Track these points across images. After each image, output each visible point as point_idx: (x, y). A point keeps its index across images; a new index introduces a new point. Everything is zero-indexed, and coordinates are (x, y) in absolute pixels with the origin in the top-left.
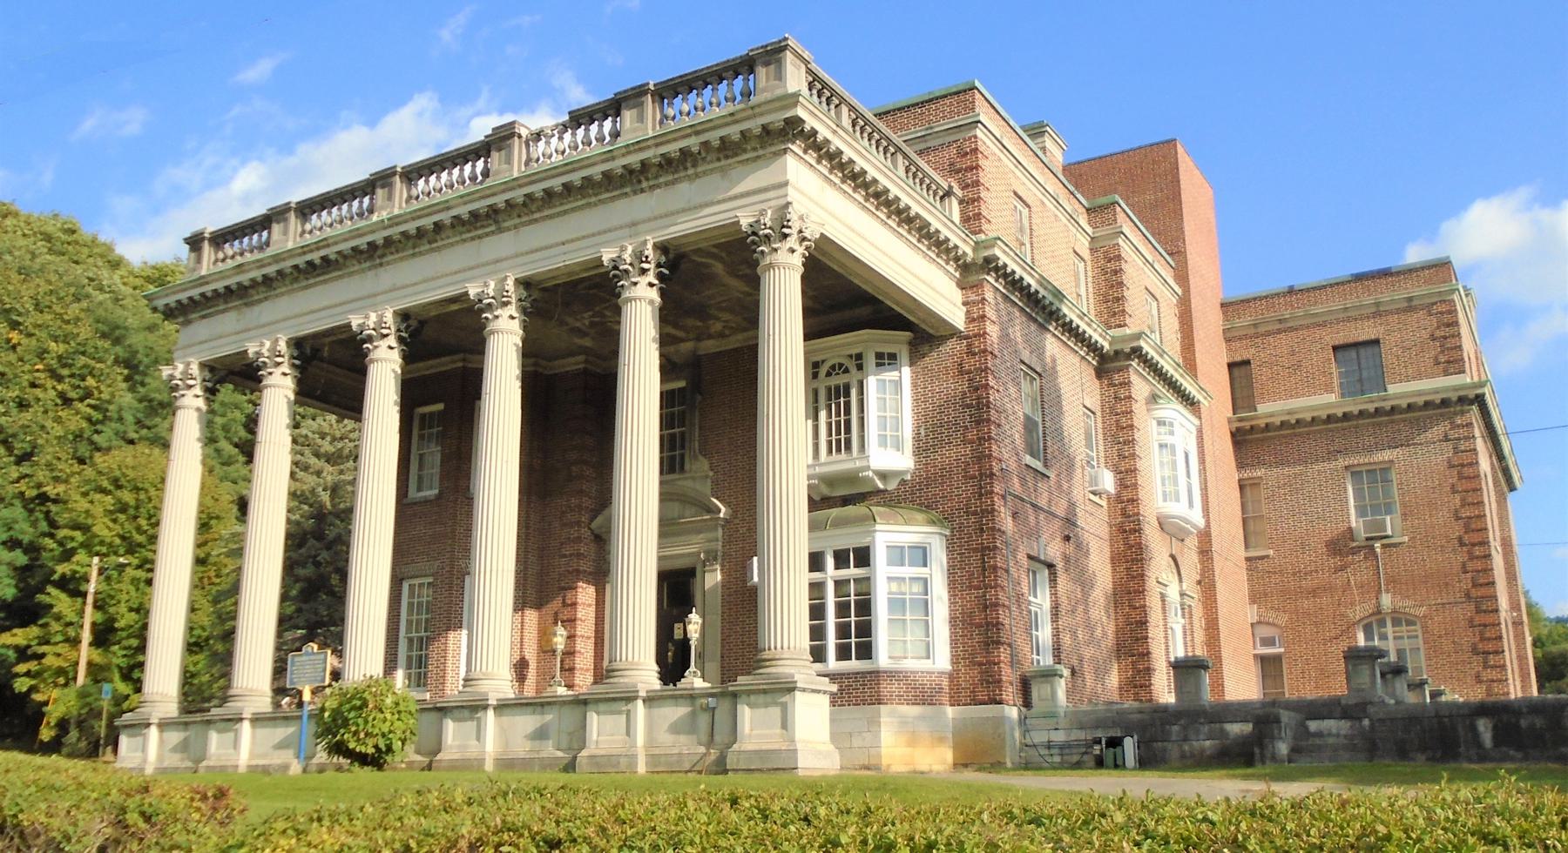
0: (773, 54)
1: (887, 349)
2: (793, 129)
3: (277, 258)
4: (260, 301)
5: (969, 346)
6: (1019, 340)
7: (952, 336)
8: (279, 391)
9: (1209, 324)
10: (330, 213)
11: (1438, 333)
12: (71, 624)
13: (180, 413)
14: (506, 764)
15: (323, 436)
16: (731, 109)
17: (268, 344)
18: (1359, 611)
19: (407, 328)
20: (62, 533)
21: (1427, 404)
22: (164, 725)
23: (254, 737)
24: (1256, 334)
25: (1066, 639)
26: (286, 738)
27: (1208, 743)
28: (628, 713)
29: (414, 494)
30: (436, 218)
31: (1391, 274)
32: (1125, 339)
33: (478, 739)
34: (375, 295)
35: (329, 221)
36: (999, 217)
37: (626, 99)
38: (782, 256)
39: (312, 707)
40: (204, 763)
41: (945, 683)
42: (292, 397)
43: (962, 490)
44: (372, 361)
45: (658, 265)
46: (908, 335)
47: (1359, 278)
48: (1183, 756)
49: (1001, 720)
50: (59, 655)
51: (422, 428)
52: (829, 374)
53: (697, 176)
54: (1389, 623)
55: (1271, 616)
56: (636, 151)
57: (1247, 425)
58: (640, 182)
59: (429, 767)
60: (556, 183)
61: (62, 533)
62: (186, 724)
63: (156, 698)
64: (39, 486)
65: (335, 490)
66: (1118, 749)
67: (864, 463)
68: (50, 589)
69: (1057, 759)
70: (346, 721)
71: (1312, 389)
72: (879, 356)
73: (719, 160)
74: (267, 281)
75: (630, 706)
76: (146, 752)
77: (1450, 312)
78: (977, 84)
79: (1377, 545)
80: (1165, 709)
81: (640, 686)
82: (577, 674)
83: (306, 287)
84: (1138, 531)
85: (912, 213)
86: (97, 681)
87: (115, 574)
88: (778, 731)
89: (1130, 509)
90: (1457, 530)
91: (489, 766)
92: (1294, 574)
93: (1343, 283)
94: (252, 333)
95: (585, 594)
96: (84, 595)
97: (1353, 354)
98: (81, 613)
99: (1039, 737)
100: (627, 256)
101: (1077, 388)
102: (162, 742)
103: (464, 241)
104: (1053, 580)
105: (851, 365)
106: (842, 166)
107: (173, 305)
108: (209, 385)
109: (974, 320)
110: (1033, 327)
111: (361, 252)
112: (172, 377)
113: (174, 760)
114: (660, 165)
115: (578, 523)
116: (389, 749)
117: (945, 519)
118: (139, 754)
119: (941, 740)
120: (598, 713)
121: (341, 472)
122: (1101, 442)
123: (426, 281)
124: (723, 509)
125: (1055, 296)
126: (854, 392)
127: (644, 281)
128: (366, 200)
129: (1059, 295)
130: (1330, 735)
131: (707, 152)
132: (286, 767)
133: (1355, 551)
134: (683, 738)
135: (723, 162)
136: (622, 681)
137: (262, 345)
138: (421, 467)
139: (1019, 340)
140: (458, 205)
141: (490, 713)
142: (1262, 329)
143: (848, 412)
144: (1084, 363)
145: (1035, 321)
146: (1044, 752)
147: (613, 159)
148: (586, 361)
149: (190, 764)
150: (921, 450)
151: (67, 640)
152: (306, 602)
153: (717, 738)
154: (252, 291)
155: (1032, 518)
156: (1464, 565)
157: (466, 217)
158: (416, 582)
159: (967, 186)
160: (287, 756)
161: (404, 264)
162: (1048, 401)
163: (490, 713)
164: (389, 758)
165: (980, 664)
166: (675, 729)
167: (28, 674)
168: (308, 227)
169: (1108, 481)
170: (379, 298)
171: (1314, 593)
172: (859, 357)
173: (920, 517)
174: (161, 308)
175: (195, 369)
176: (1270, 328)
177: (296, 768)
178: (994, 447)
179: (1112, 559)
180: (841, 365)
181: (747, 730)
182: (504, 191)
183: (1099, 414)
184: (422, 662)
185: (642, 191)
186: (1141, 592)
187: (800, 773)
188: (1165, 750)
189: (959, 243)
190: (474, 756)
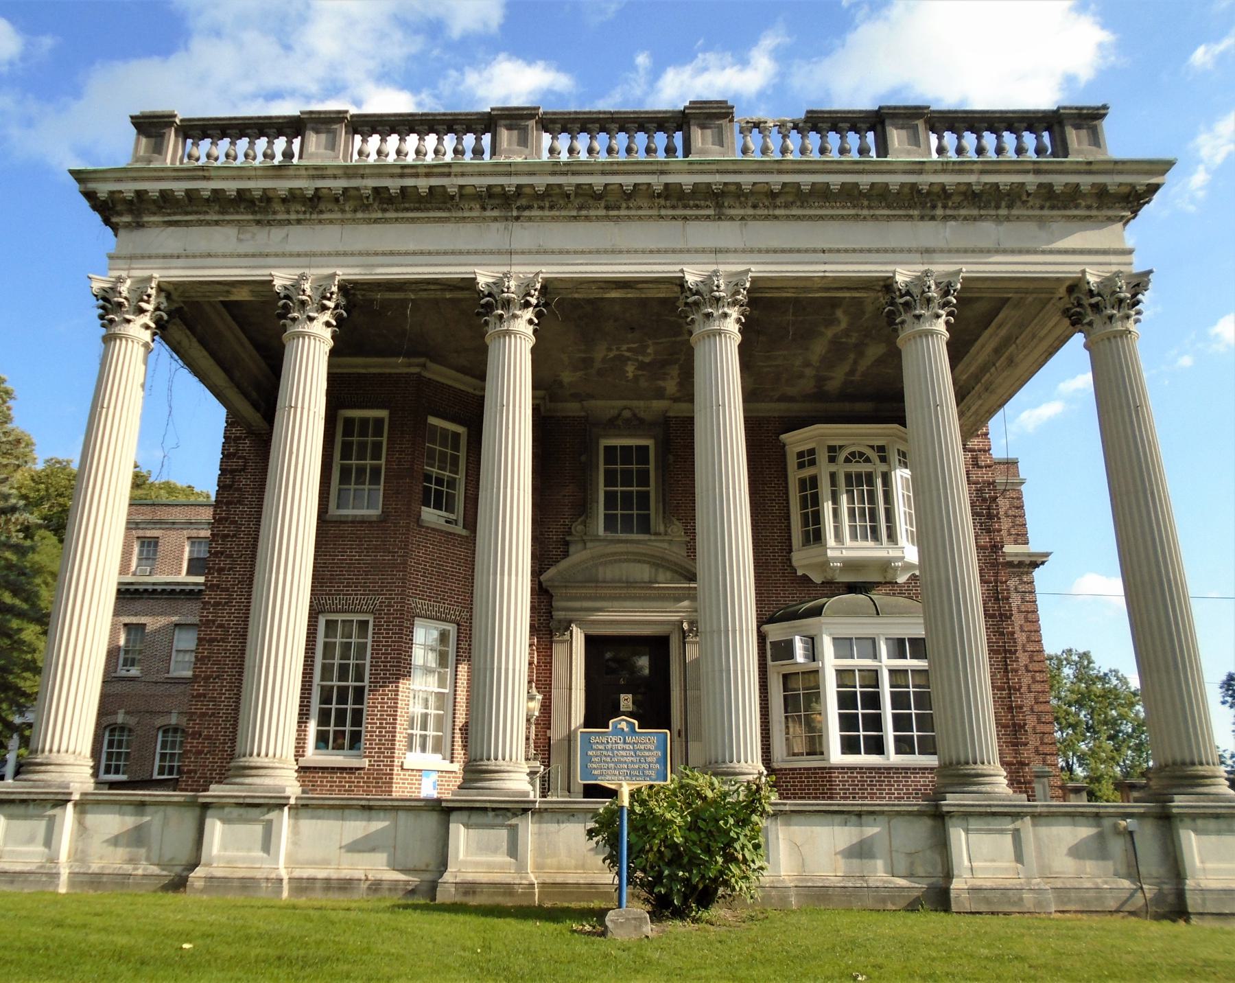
11: (1010, 513)
23: (295, 831)
26: (367, 837)
28: (52, 819)
29: (333, 511)
45: (157, 309)
52: (847, 460)
53: (1008, 218)
56: (953, 172)
58: (934, 207)
73: (1042, 208)
75: (1018, 824)
83: (376, 221)
103: (661, 217)
105: (873, 455)
120: (967, 831)
134: (1090, 866)
135: (1046, 212)
140: (680, 172)
143: (872, 499)
147: (920, 172)
161: (364, 228)
166: (1076, 852)
172: (881, 449)
180: (861, 454)
185: (933, 218)
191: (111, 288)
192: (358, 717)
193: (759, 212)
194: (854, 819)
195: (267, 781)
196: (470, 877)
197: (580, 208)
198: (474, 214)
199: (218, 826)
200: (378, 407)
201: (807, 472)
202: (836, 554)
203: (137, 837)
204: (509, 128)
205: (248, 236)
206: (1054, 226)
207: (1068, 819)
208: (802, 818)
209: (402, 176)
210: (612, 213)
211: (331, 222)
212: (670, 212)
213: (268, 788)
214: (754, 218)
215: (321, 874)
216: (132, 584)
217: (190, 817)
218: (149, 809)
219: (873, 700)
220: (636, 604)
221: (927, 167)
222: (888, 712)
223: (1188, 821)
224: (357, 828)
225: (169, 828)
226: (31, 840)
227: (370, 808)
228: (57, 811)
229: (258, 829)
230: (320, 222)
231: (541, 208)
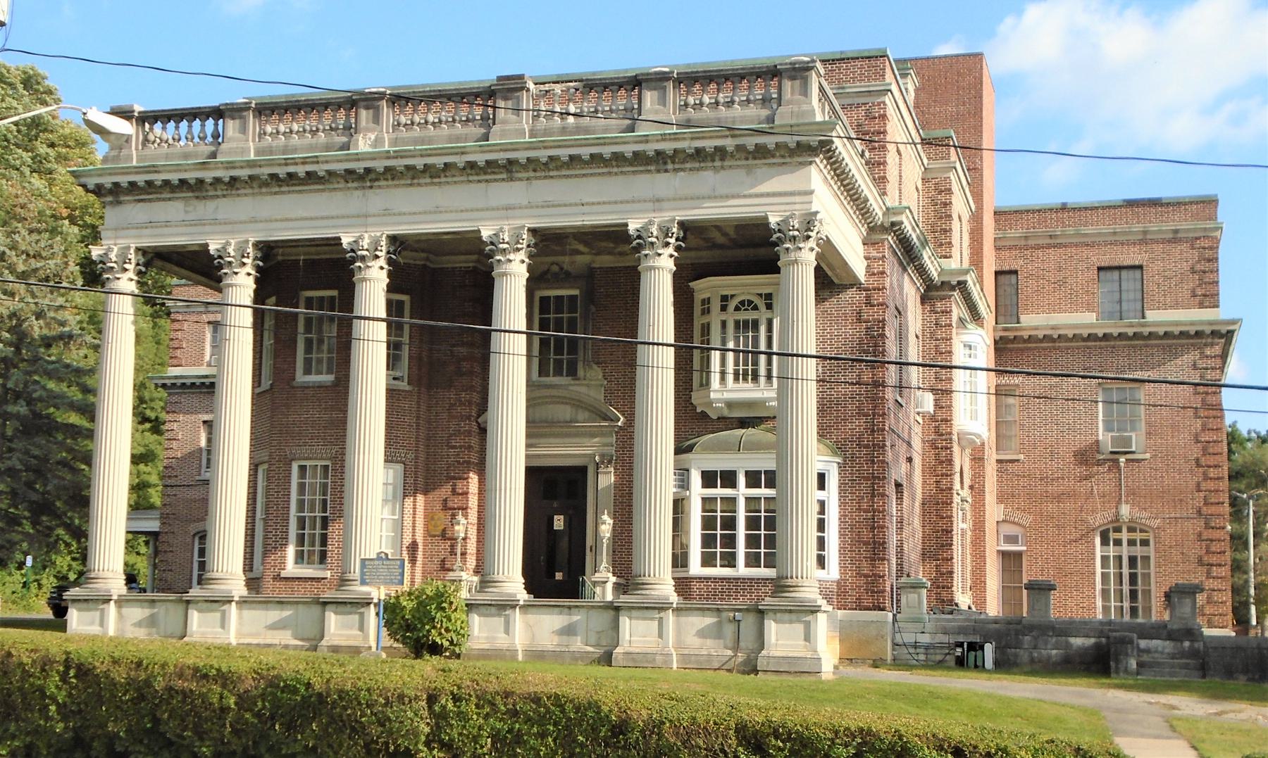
2: (824, 148)
5: (868, 297)
7: (852, 286)
11: (1198, 267)
18: (1100, 519)
21: (1183, 334)
23: (240, 617)
24: (1025, 246)
27: (1054, 652)
31: (1162, 205)
47: (1131, 204)
48: (1032, 661)
52: (737, 309)
53: (722, 168)
54: (1124, 530)
57: (1011, 335)
58: (665, 163)
66: (979, 653)
69: (922, 657)
71: (1075, 307)
73: (747, 159)
75: (662, 614)
77: (1211, 248)
79: (1122, 460)
83: (276, 193)
88: (803, 643)
90: (1196, 451)
92: (1041, 479)
93: (1115, 207)
97: (1116, 274)
99: (909, 638)
105: (761, 303)
109: (874, 274)
115: (469, 418)
120: (630, 618)
126: (763, 329)
130: (1156, 652)
133: (1099, 463)
134: (709, 642)
135: (751, 162)
142: (1031, 242)
146: (912, 650)
147: (647, 142)
156: (1198, 485)
158: (307, 463)
165: (866, 576)
166: (702, 634)
170: (370, 220)
171: (1059, 498)
172: (769, 296)
176: (1040, 242)
180: (750, 302)
181: (773, 640)
185: (666, 171)
188: (1016, 655)
190: (505, 646)
192: (324, 541)
193: (538, 174)
195: (222, 587)
196: (336, 643)
197: (413, 178)
198: (340, 186)
199: (195, 613)
200: (330, 288)
201: (705, 320)
202: (718, 396)
203: (151, 622)
204: (367, 108)
205: (190, 209)
206: (759, 171)
208: (534, 610)
209: (286, 165)
212: (476, 178)
213: (223, 591)
214: (536, 178)
215: (255, 641)
216: (206, 377)
217: (181, 607)
218: (158, 604)
219: (730, 523)
220: (557, 440)
222: (741, 532)
223: (771, 614)
224: (275, 615)
225: (168, 612)
226: (92, 623)
227: (282, 603)
228: (105, 606)
229: (218, 615)
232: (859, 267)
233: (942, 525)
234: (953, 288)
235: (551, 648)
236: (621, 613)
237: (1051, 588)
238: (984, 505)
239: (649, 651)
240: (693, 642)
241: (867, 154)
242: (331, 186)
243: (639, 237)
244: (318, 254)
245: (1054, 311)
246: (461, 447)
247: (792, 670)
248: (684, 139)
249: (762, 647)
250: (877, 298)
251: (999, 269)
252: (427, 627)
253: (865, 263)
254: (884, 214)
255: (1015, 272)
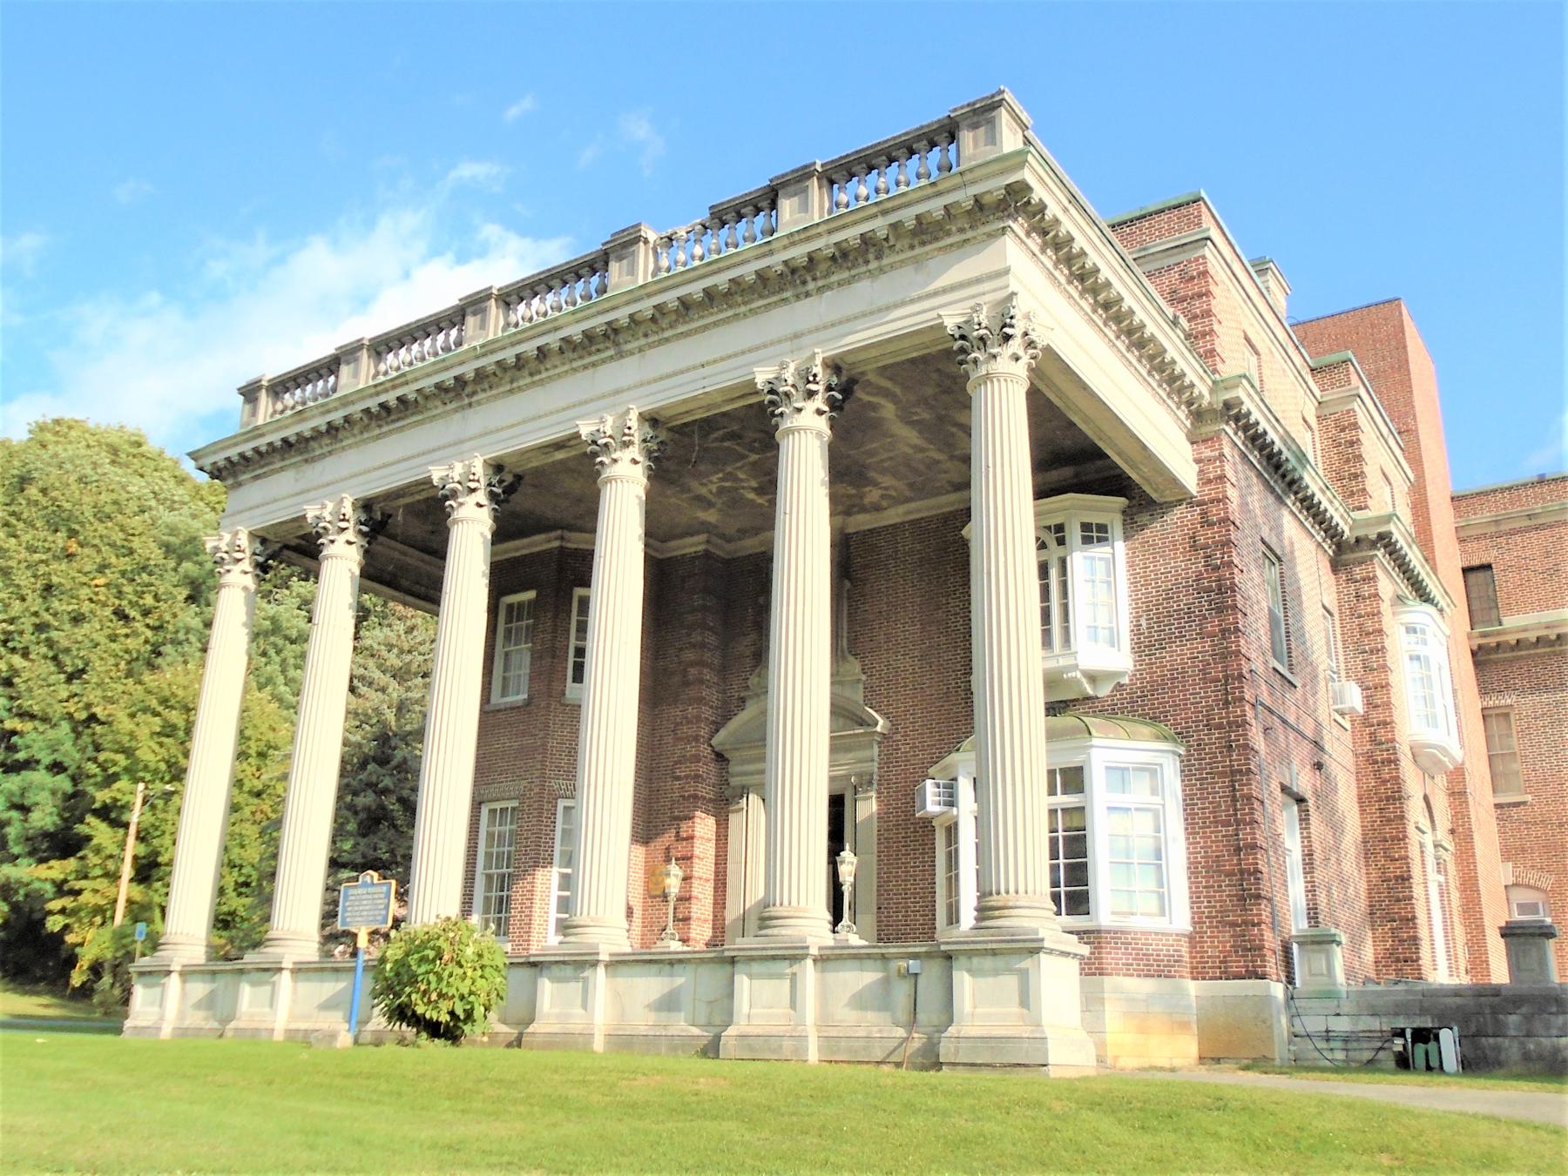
0: (984, 112)
1: (1095, 519)
2: (1016, 201)
3: (345, 401)
4: (323, 456)
5: (1204, 514)
6: (1258, 512)
7: (1180, 502)
8: (343, 560)
9: (1443, 520)
10: (409, 350)
12: (111, 856)
13: (224, 592)
14: (622, 1042)
15: (390, 647)
16: (930, 179)
17: (330, 506)
19: (501, 482)
20: (102, 757)
22: (187, 974)
23: (295, 991)
24: (1499, 532)
25: (1322, 899)
29: (496, 699)
30: (540, 342)
32: (1368, 523)
33: (584, 1006)
34: (461, 442)
35: (408, 359)
36: (1234, 360)
37: (785, 184)
38: (1003, 365)
39: (367, 957)
40: (232, 1025)
41: (1185, 950)
42: (357, 572)
43: (1203, 696)
44: (456, 522)
45: (829, 388)
46: (1121, 502)
48: (1527, 1057)
49: (1268, 999)
50: (96, 891)
51: (509, 620)
53: (881, 270)
55: (1532, 877)
57: (1492, 641)
58: (804, 283)
59: (518, 1042)
60: (695, 289)
61: (102, 757)
62: (214, 973)
63: (180, 939)
64: (88, 706)
65: (401, 708)
66: (1432, 1046)
67: (1071, 661)
68: (89, 818)
69: (1340, 1055)
70: (413, 980)
72: (1086, 527)
73: (912, 247)
74: (332, 430)
75: (796, 968)
76: (160, 1008)
78: (1203, 194)
80: (1496, 991)
81: (809, 941)
82: (694, 924)
83: (378, 437)
84: (1393, 761)
85: (1147, 333)
86: (136, 921)
87: (160, 803)
88: (1015, 1009)
89: (1382, 734)
91: (599, 1045)
94: (312, 495)
95: (704, 826)
96: (126, 826)
98: (122, 845)
99: (1315, 1024)
100: (789, 375)
101: (1315, 581)
102: (184, 995)
103: (575, 370)
104: (1304, 819)
106: (1069, 260)
107: (221, 464)
108: (261, 559)
109: (1210, 481)
110: (1271, 499)
111: (447, 390)
112: (217, 549)
113: (197, 1019)
114: (833, 258)
115: (696, 738)
116: (469, 1015)
117: (1181, 735)
118: (156, 1009)
119: (1184, 1026)
120: (751, 977)
121: (408, 689)
122: (1341, 650)
123: (523, 423)
124: (881, 722)
125: (1299, 461)
127: (811, 406)
128: (454, 333)
129: (1302, 458)
131: (898, 238)
132: (333, 1036)
134: (871, 1016)
135: (918, 251)
136: (787, 933)
137: (324, 507)
138: (506, 669)
139: (1258, 512)
140: (568, 325)
141: (601, 970)
142: (1504, 527)
144: (1320, 552)
145: (1272, 491)
146: (1322, 1045)
147: (771, 253)
148: (708, 542)
149: (216, 1025)
150: (1144, 645)
151: (106, 875)
152: (364, 836)
153: (922, 1016)
154: (313, 444)
155: (1282, 738)
157: (578, 338)
158: (498, 806)
159: (1195, 317)
160: (335, 1022)
162: (1287, 594)
163: (601, 970)
164: (467, 1028)
165: (1233, 925)
166: (860, 1001)
167: (63, 911)
168: (382, 367)
169: (1354, 698)
170: (467, 446)
172: (1060, 528)
173: (1146, 730)
174: (208, 468)
175: (244, 540)
176: (1516, 525)
177: (345, 1039)
178: (1242, 642)
179: (1360, 798)
182: (627, 303)
183: (1337, 616)
184: (503, 904)
185: (807, 295)
186: (1401, 838)
187: (1053, 1072)
188: (1497, 1049)
189: (1196, 381)
190: (577, 1029)
191: (966, 322)
193: (651, 339)
194: (668, 967)
197: (512, 382)
207: (857, 963)
210: (537, 378)
211: (350, 446)
214: (651, 346)
221: (774, 245)
230: (343, 448)
231: (484, 390)
232: (1188, 476)
233: (1393, 870)
234: (1373, 545)
235: (643, 1030)
236: (739, 967)
237: (1547, 933)
238: (1473, 855)
239: (774, 1031)
240: (847, 1017)
241: (1183, 321)
242: (430, 414)
243: (772, 392)
244: (517, 550)
245: (1548, 607)
246: (687, 777)
247: (998, 1060)
248: (820, 235)
249: (951, 1021)
250: (1215, 513)
251: (1467, 564)
252: (408, 990)
253: (1196, 467)
254: (1212, 392)
255: (1488, 567)
